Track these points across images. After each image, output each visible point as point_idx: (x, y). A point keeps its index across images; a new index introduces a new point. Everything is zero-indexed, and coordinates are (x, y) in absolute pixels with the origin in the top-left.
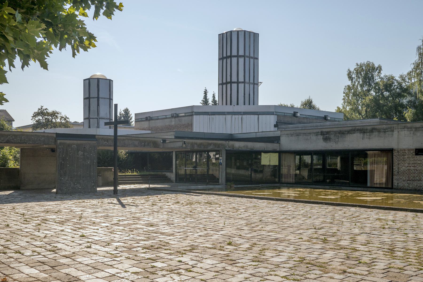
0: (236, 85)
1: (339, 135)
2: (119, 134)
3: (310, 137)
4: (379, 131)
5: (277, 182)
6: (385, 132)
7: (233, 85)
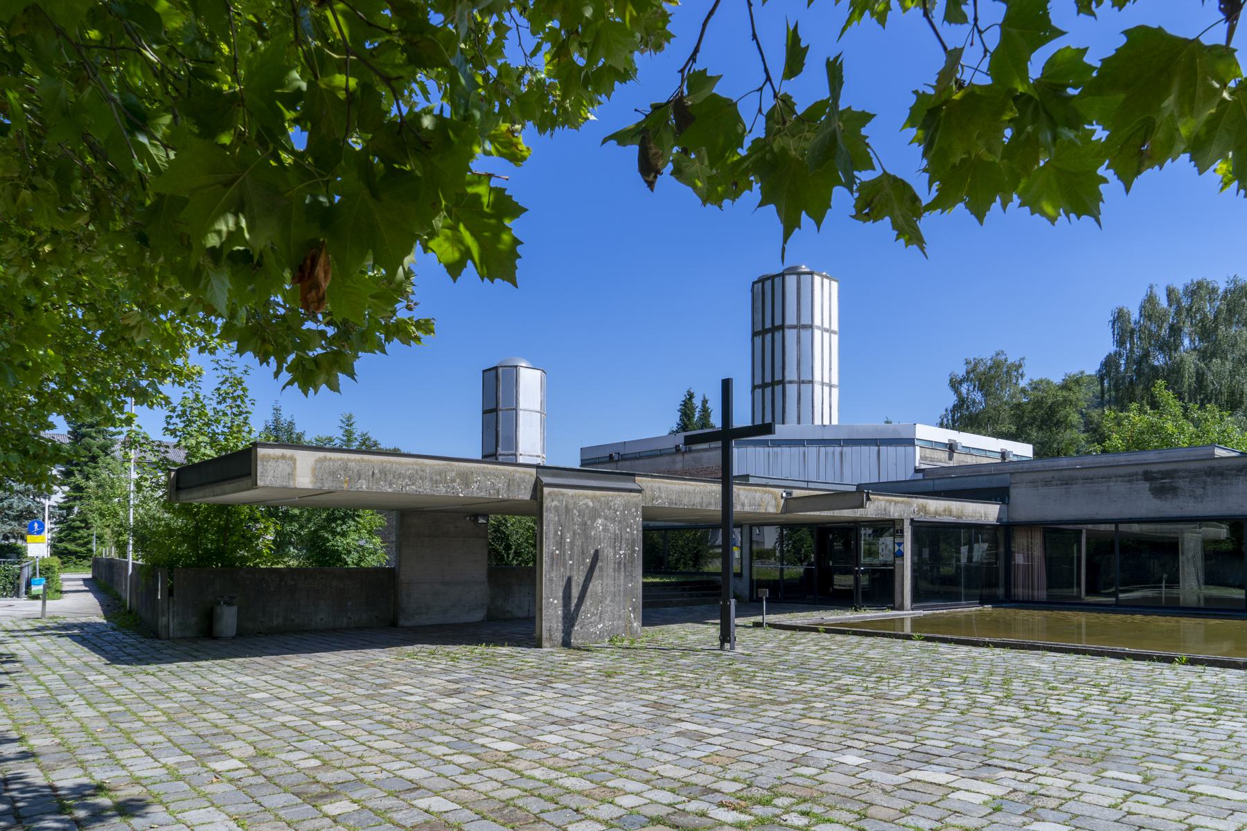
0: (795, 386)
1: (1209, 480)
3: (1109, 486)
5: (1001, 598)
7: (803, 386)
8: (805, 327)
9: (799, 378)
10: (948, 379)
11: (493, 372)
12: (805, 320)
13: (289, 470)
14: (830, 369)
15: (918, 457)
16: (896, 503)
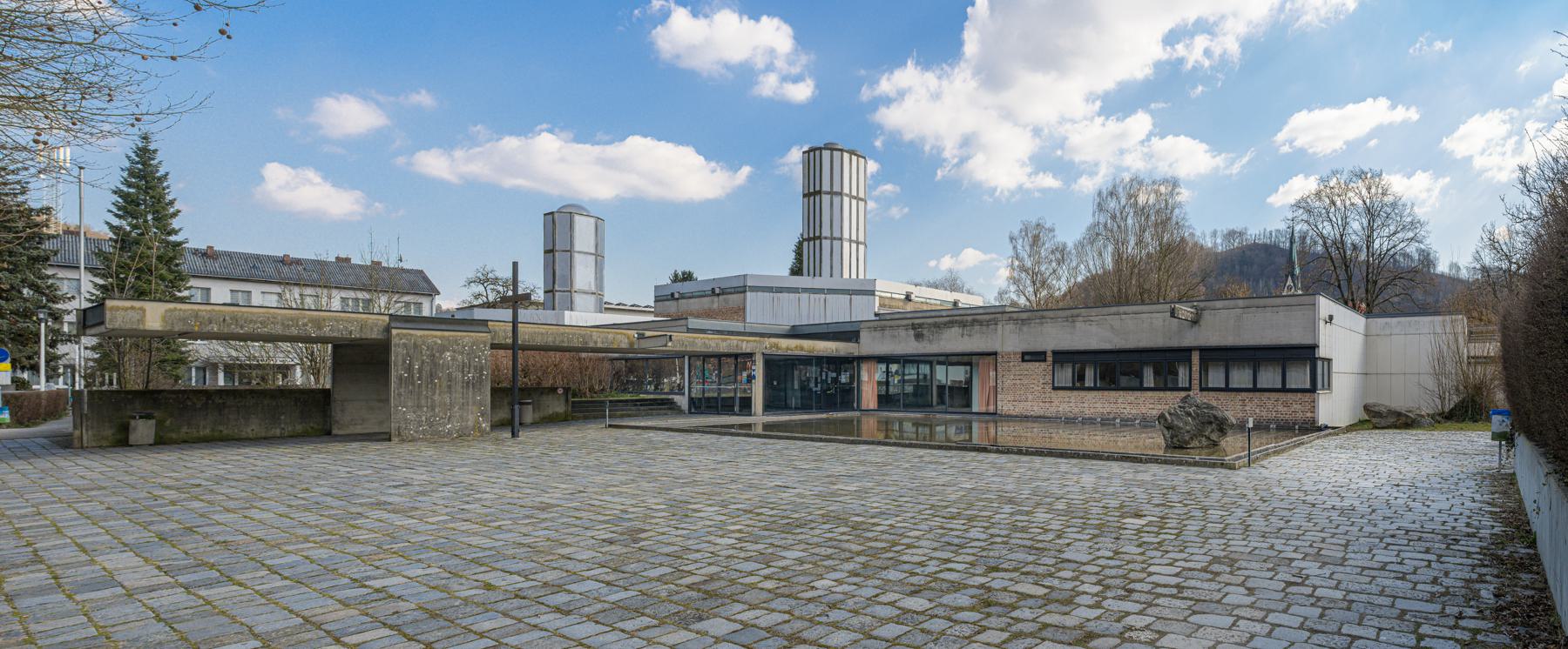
0: (828, 242)
2: (510, 311)
4: (981, 323)
6: (988, 325)
7: (835, 242)
8: (836, 193)
9: (832, 234)
10: (1007, 235)
11: (551, 216)
12: (836, 188)
13: (138, 317)
14: (858, 229)
15: (877, 304)
16: (747, 341)
